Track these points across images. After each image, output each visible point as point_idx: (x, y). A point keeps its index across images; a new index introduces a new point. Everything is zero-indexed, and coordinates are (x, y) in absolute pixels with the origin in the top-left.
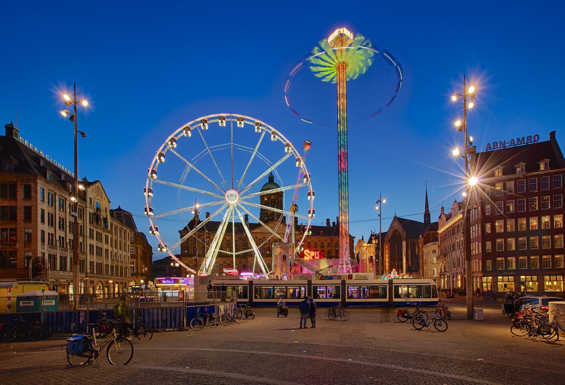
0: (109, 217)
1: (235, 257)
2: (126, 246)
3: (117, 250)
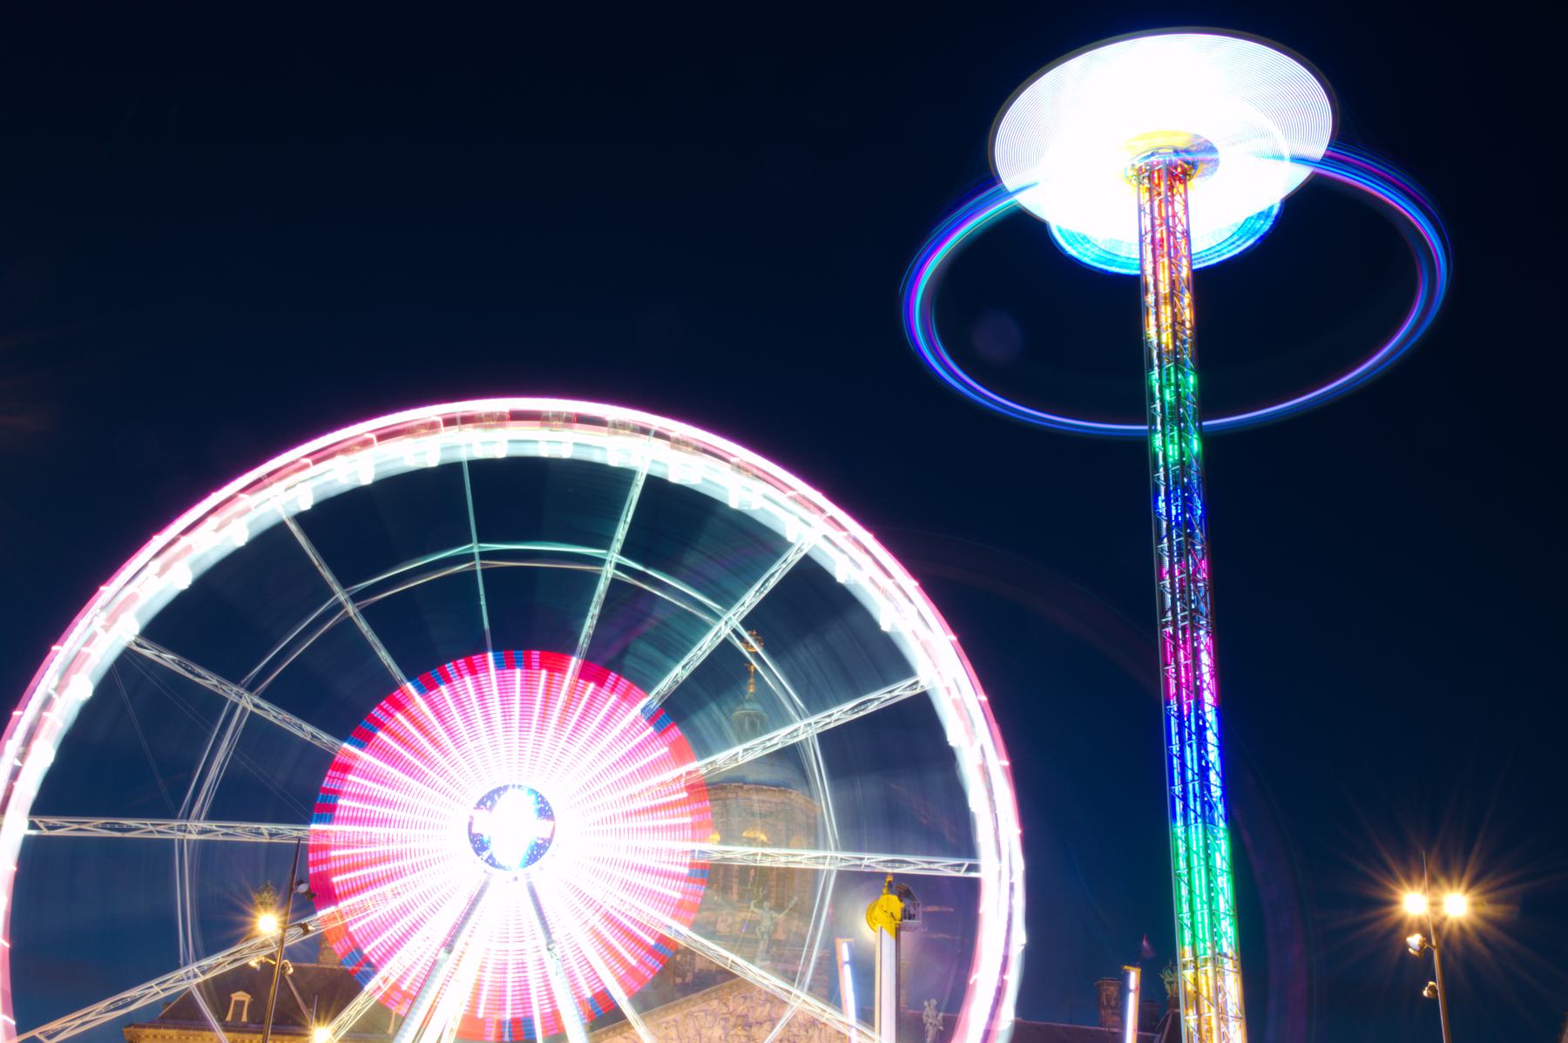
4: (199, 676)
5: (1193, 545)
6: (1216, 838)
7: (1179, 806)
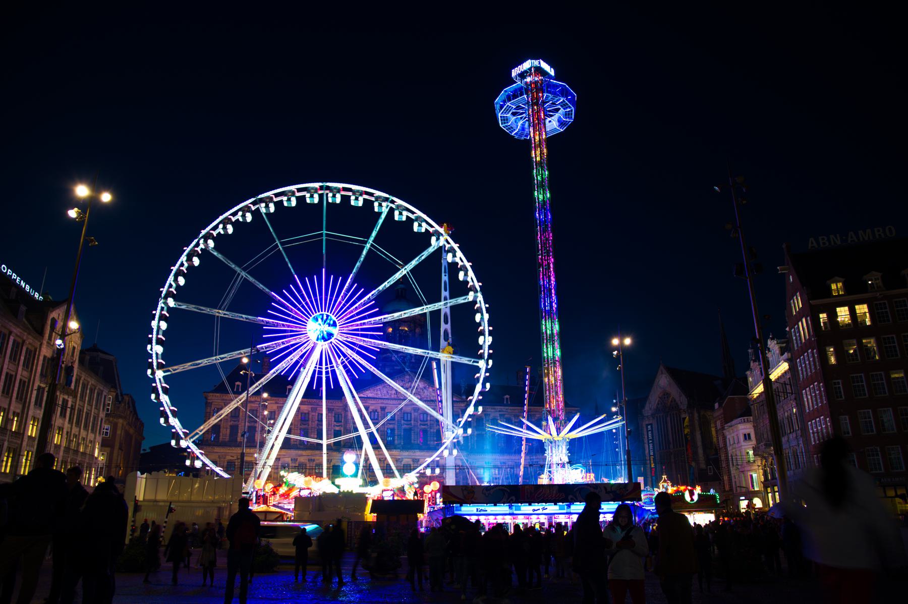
0: (76, 366)
1: (328, 449)
2: (98, 421)
3: (78, 429)
4: (229, 263)
5: (548, 228)
6: (555, 324)
7: (545, 341)
